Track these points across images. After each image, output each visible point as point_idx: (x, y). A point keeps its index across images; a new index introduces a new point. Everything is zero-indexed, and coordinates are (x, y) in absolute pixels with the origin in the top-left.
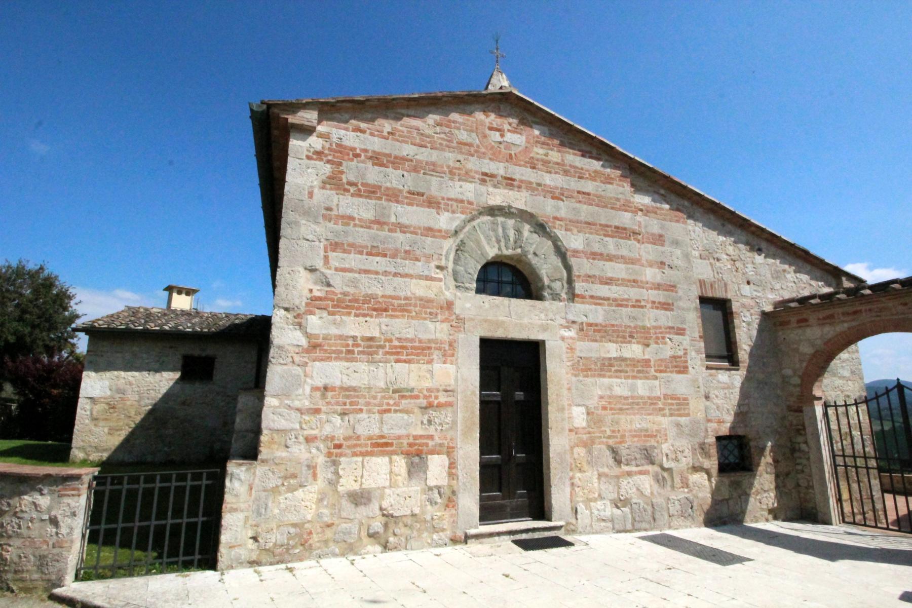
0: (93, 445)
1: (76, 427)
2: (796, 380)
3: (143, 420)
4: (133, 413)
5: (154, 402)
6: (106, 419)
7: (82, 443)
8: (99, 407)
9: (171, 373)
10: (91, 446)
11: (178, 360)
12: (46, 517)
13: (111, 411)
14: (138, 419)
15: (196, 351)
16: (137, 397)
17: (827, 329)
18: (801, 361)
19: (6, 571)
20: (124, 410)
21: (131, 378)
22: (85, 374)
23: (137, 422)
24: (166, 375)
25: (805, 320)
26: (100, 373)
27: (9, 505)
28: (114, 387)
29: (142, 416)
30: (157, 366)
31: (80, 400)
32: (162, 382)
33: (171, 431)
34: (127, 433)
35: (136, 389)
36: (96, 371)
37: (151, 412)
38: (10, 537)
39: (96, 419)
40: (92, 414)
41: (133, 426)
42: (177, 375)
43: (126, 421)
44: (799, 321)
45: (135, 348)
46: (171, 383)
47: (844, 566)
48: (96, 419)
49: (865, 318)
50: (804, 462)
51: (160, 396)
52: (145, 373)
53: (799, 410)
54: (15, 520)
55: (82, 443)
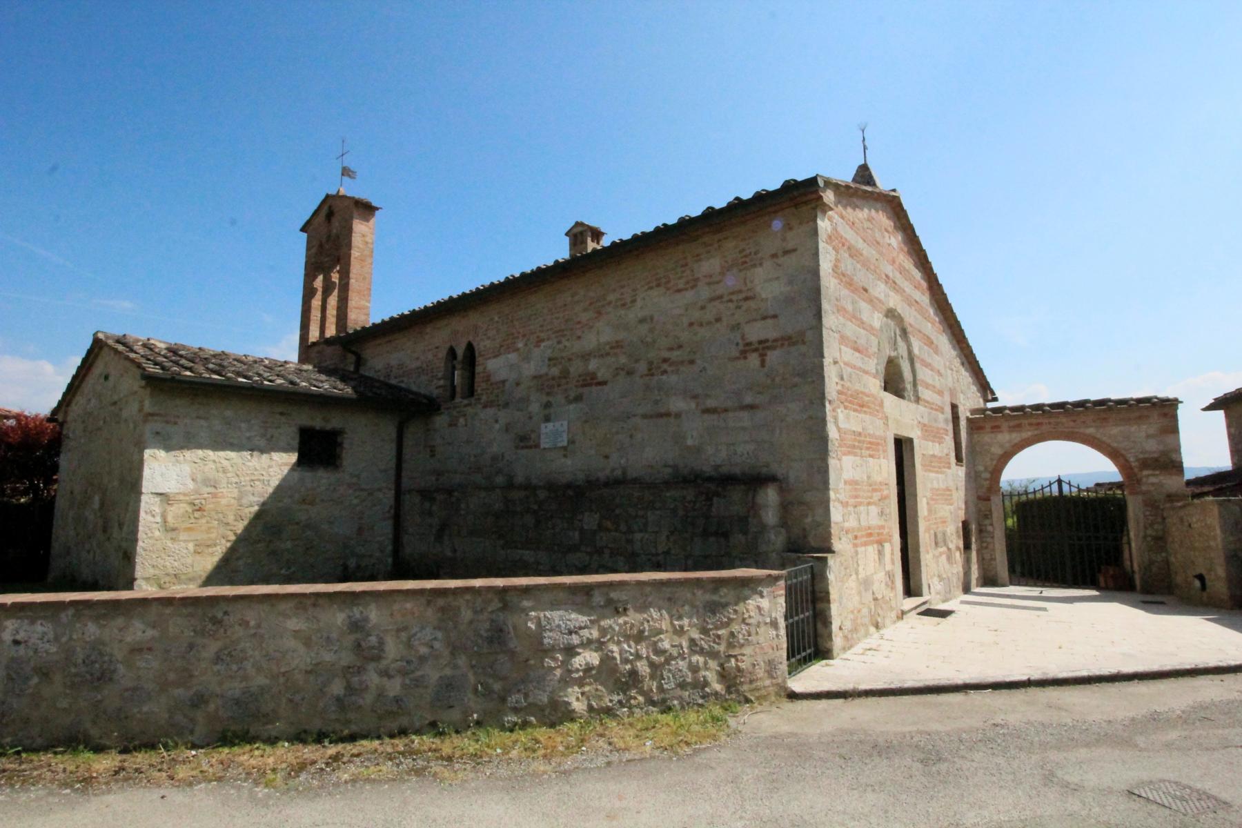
0: (171, 571)
1: (140, 543)
2: (987, 475)
3: (247, 529)
4: (231, 518)
5: (262, 500)
6: (190, 529)
7: (152, 571)
8: (174, 511)
9: (284, 455)
10: (168, 575)
11: (289, 432)
12: (768, 620)
13: (197, 514)
14: (240, 527)
15: (316, 420)
16: (236, 493)
17: (1014, 435)
18: (992, 460)
19: (742, 683)
20: (217, 513)
21: (225, 463)
22: (148, 453)
23: (239, 532)
24: (277, 456)
25: (998, 427)
26: (173, 453)
27: (736, 611)
28: (199, 477)
29: (246, 522)
30: (262, 443)
31: (144, 498)
32: (276, 466)
33: (289, 545)
34: (224, 550)
35: (234, 480)
36: (168, 449)
37: (258, 516)
38: (742, 646)
39: (174, 530)
40: (165, 521)
41: (233, 538)
42: (293, 458)
43: (222, 530)
44: (993, 428)
45: (228, 413)
46: (286, 470)
47: (1078, 605)
48: (174, 530)
49: (1045, 428)
50: (989, 540)
51: (271, 490)
52: (246, 454)
53: (988, 499)
54: (743, 626)
55: (152, 571)
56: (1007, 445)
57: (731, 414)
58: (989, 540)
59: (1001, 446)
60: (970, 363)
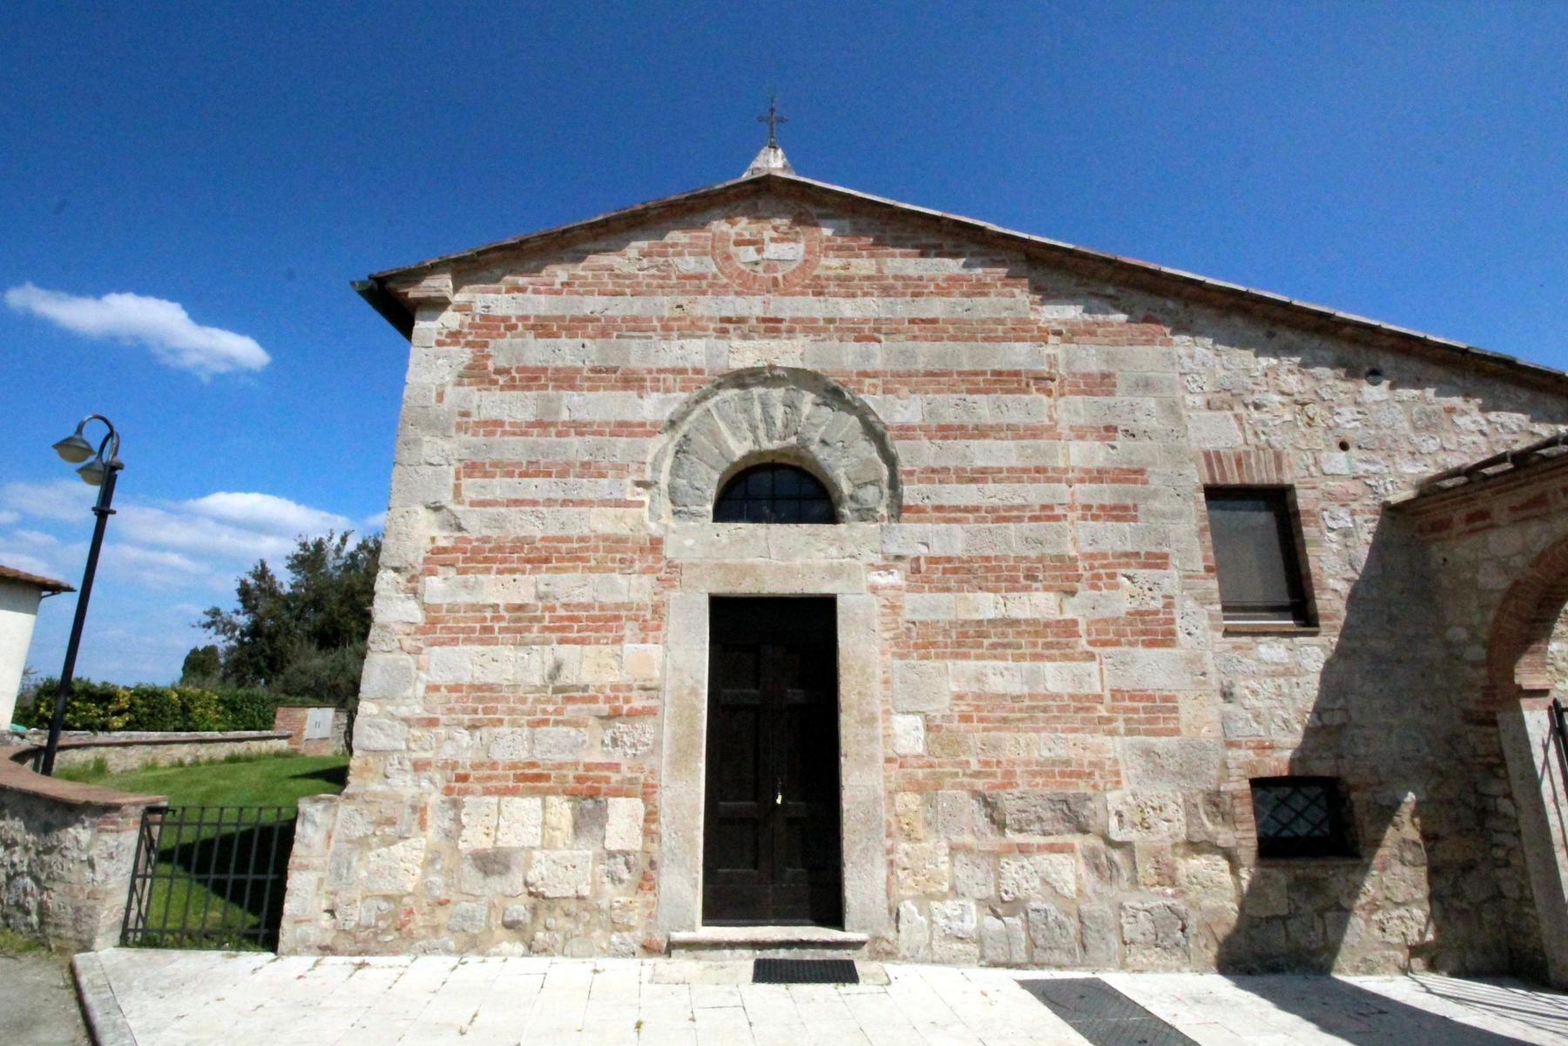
17: (1534, 529)
18: (1484, 608)
25: (1484, 515)
44: (1471, 518)
50: (1509, 840)
56: (1518, 561)
57: (595, 510)
58: (1509, 840)
59: (1505, 569)
60: (691, 210)
